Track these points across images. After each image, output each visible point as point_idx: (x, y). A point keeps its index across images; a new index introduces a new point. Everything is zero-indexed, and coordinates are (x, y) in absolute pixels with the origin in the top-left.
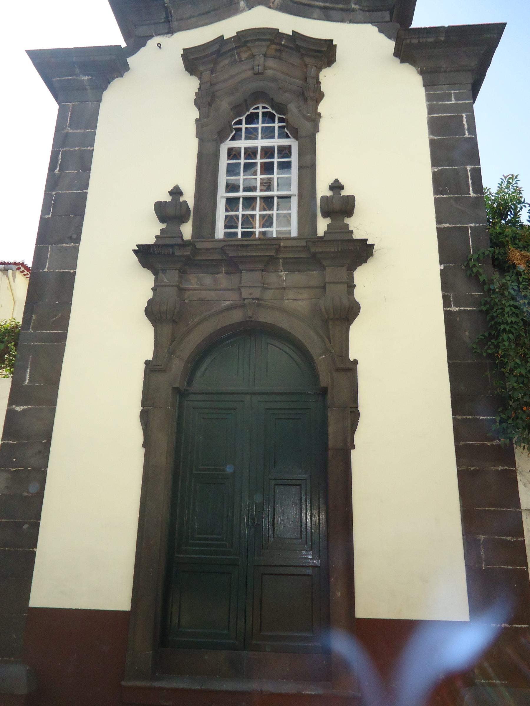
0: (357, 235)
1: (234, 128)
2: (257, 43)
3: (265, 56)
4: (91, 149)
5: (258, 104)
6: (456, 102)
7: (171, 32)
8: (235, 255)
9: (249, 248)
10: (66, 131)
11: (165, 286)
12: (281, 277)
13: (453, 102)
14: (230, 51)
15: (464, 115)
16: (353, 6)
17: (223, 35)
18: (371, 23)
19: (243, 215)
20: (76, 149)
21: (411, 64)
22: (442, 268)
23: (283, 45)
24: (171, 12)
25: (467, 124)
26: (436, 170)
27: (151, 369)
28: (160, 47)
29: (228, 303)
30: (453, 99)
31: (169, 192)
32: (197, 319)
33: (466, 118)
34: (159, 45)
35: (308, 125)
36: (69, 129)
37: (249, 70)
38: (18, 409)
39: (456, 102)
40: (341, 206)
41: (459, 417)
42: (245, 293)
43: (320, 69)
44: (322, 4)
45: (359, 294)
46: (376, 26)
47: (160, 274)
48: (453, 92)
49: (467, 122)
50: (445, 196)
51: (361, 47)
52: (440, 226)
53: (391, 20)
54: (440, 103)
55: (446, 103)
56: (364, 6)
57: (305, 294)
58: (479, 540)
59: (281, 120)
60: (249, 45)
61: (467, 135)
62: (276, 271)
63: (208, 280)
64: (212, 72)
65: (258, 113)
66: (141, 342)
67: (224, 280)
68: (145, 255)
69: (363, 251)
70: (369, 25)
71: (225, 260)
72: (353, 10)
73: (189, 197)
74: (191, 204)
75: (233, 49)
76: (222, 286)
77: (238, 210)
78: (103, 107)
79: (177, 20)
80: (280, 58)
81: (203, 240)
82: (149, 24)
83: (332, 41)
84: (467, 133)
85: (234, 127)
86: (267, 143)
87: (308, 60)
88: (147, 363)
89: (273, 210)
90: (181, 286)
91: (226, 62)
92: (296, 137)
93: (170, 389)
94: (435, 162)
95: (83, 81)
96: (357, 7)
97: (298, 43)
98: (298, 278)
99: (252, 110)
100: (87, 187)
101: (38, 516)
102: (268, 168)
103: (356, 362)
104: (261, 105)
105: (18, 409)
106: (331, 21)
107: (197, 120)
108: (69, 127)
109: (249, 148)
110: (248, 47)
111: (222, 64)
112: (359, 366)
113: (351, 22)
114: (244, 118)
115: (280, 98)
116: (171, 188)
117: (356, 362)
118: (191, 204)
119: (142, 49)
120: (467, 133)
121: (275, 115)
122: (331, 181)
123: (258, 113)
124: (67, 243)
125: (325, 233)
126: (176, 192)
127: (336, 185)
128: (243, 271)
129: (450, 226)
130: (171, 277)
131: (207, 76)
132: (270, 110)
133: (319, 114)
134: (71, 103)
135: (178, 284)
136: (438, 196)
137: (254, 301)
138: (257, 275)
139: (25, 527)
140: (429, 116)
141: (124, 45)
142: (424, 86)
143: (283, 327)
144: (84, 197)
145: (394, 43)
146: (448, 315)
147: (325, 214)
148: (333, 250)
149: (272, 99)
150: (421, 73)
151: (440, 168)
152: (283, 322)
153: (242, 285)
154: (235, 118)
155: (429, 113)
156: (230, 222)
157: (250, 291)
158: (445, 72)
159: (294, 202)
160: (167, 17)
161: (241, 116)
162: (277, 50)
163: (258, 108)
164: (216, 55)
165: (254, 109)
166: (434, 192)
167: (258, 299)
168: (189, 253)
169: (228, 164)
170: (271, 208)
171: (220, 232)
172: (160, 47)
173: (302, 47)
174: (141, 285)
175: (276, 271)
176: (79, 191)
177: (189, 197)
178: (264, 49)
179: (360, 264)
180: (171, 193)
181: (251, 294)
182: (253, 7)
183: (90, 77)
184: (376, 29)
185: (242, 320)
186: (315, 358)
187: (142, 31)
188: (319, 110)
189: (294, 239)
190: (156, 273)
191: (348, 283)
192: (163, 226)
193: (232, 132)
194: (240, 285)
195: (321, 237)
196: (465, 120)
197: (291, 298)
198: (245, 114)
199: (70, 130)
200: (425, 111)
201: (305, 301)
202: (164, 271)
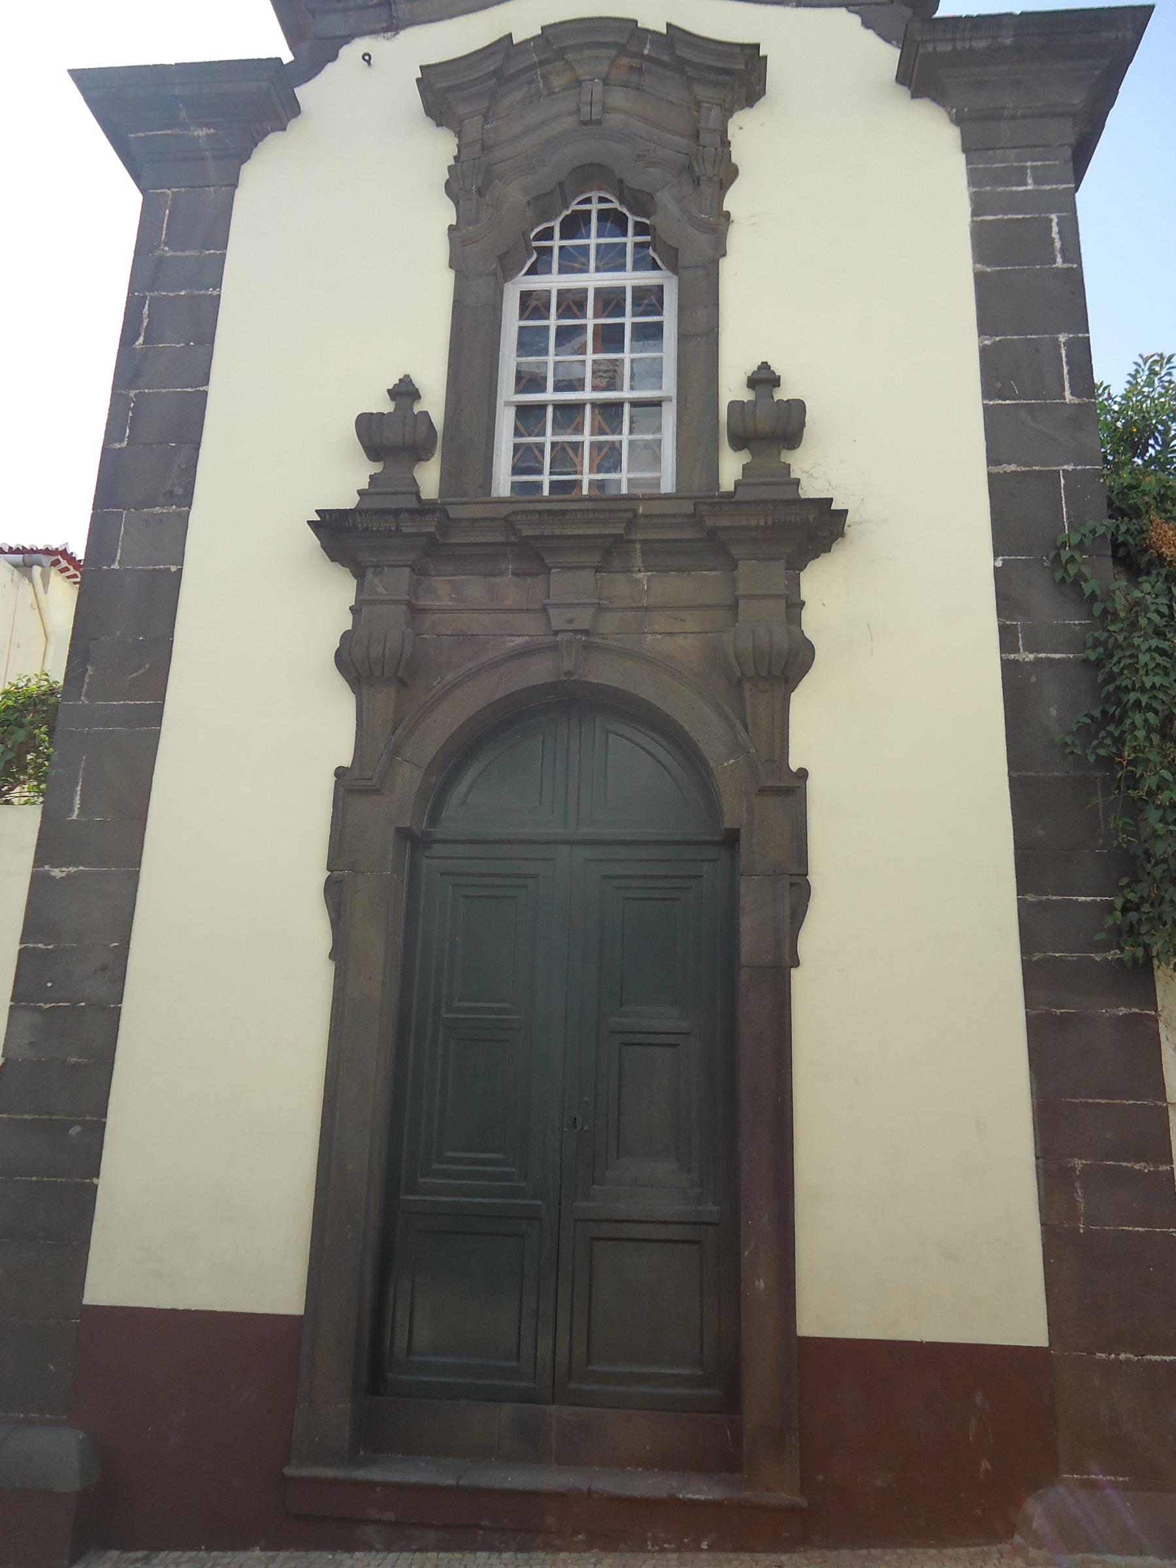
0: (810, 490)
1: (536, 248)
2: (587, 53)
4: (215, 293)
8: (537, 533)
11: (381, 602)
12: (638, 582)
13: (1030, 187)
15: (1054, 217)
18: (846, 6)
19: (553, 444)
20: (182, 293)
22: (999, 564)
25: (1061, 239)
26: (987, 342)
28: (369, 62)
30: (1030, 181)
34: (367, 58)
35: (702, 239)
38: (57, 873)
40: (774, 424)
41: (1030, 898)
42: (558, 619)
43: (728, 113)
46: (856, 13)
48: (1029, 164)
49: (1059, 233)
50: (1007, 402)
52: (995, 470)
54: (1000, 189)
55: (1014, 189)
58: (1073, 1169)
59: (641, 229)
60: (569, 56)
62: (628, 571)
63: (475, 588)
64: (486, 118)
65: (589, 212)
66: (327, 727)
67: (511, 589)
68: (336, 532)
69: (822, 526)
71: (512, 544)
73: (433, 402)
75: (532, 67)
77: (542, 433)
81: (464, 499)
83: (757, 47)
84: (1059, 259)
85: (535, 244)
86: (609, 279)
87: (702, 92)
88: (340, 772)
89: (621, 433)
90: (414, 601)
91: (518, 95)
92: (674, 268)
99: (574, 207)
101: (102, 1111)
102: (610, 338)
103: (803, 774)
104: (595, 195)
105: (57, 873)
108: (166, 244)
109: (568, 291)
110: (567, 62)
112: (811, 783)
114: (556, 224)
116: (392, 381)
117: (803, 774)
120: (1059, 259)
123: (589, 212)
124: (163, 507)
125: (737, 484)
126: (404, 392)
127: (764, 375)
132: (616, 205)
133: (728, 214)
135: (407, 597)
138: (586, 578)
139: (75, 1130)
141: (287, 57)
142: (964, 151)
144: (201, 400)
145: (899, 52)
147: (739, 442)
148: (754, 523)
150: (957, 120)
151: (998, 339)
152: (644, 685)
154: (537, 225)
155: (974, 213)
156: (526, 460)
158: (1013, 118)
159: (669, 415)
161: (551, 220)
162: (631, 69)
163: (588, 201)
164: (494, 80)
167: (586, 632)
168: (432, 529)
169: (521, 328)
171: (503, 482)
172: (369, 62)
174: (326, 602)
177: (433, 402)
178: (603, 68)
181: (571, 621)
183: (212, 131)
184: (856, 19)
188: (727, 205)
189: (667, 497)
190: (359, 574)
191: (787, 597)
192: (376, 468)
193: (530, 255)
194: (547, 601)
195: (729, 495)
196: (1055, 229)
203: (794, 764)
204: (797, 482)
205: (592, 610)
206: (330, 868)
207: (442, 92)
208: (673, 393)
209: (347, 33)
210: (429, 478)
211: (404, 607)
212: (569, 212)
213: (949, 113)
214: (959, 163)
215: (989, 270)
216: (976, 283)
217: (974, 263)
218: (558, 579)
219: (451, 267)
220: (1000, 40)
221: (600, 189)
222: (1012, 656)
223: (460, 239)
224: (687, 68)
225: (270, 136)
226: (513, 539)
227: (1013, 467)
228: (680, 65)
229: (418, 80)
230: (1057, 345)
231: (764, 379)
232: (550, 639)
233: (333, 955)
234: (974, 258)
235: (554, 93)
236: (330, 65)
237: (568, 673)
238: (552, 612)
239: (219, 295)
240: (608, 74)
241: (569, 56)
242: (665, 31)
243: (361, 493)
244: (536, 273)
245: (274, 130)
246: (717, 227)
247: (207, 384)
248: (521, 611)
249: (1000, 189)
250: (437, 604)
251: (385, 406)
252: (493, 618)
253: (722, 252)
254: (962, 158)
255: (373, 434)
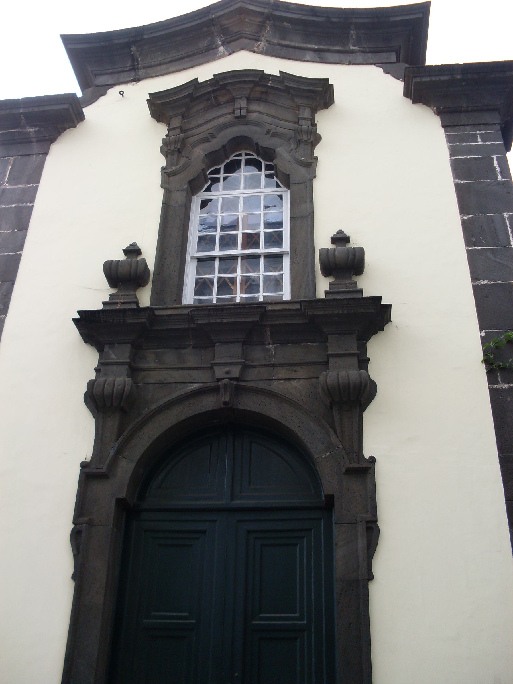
1: (210, 179)
2: (238, 86)
3: (249, 100)
4: (31, 205)
5: (241, 150)
6: (483, 143)
7: (137, 80)
8: (207, 321)
9: (225, 312)
10: (3, 187)
11: (112, 364)
12: (269, 350)
13: (480, 143)
14: (204, 94)
16: (352, 48)
17: (197, 79)
18: (375, 64)
19: (219, 279)
20: (13, 206)
21: (424, 104)
22: (483, 334)
23: (269, 86)
24: (137, 60)
25: (499, 167)
26: (465, 218)
27: (90, 475)
28: (122, 95)
29: (196, 386)
30: (479, 140)
31: (124, 250)
32: (154, 407)
33: (497, 160)
34: (122, 93)
35: (302, 170)
36: (7, 185)
37: (229, 113)
39: (483, 143)
40: (346, 262)
42: (219, 372)
43: (314, 111)
44: (316, 47)
45: (375, 372)
46: (380, 67)
47: (106, 349)
48: (478, 132)
49: (498, 164)
50: (479, 248)
51: (364, 93)
52: (476, 283)
53: (398, 61)
54: (464, 144)
55: (471, 144)
56: (365, 48)
57: (302, 372)
59: (268, 168)
60: (229, 88)
61: (500, 178)
62: (262, 344)
63: (170, 357)
64: (184, 117)
65: (240, 160)
67: (191, 358)
68: (89, 324)
70: (373, 68)
72: (352, 52)
73: (149, 256)
74: (151, 265)
75: (209, 93)
76: (189, 364)
77: (212, 272)
78: (49, 160)
79: (145, 68)
80: (266, 101)
81: (165, 306)
82: (111, 73)
83: (327, 80)
84: (500, 176)
85: (210, 176)
87: (298, 101)
89: (259, 271)
91: (202, 106)
92: (287, 185)
93: (114, 501)
94: (463, 209)
95: (28, 133)
96: (356, 48)
97: (286, 84)
98: (295, 353)
99: (232, 158)
100: (21, 248)
103: (372, 460)
104: (243, 152)
106: (327, 63)
107: (163, 169)
108: (7, 183)
110: (227, 90)
111: (195, 109)
113: (350, 64)
114: (222, 167)
115: (266, 142)
116: (126, 245)
117: (372, 460)
118: (151, 265)
119: (102, 98)
120: (500, 176)
121: (261, 163)
122: (333, 232)
123: (240, 160)
125: (326, 293)
126: (133, 251)
127: (339, 236)
128: (217, 344)
129: (489, 283)
130: (121, 353)
131: (176, 122)
132: (255, 156)
133: (316, 158)
134: (12, 157)
135: (128, 360)
136: (470, 248)
137: (232, 382)
138: (237, 349)
140: (452, 158)
141: (79, 94)
142: (443, 126)
143: (272, 416)
144: (17, 259)
145: (402, 83)
146: (494, 394)
147: (327, 271)
148: (336, 312)
149: (257, 144)
150: (439, 113)
151: (471, 216)
152: (272, 410)
153: (217, 361)
154: (211, 167)
155: (451, 155)
156: (203, 287)
157: (227, 369)
158: (467, 111)
159: (287, 262)
160: (133, 65)
161: (219, 164)
162: (262, 93)
163: (240, 155)
164: (188, 99)
165: (234, 156)
166: (465, 243)
167: (237, 379)
168: (144, 320)
170: (256, 268)
171: (189, 298)
172: (122, 95)
173: (292, 88)
174: (82, 363)
175: (262, 344)
176: (12, 254)
177: (149, 256)
178: (247, 92)
179: (375, 333)
180: (127, 252)
181: (227, 373)
182: (234, 52)
183: (38, 129)
184: (381, 70)
185: (215, 408)
186: (316, 456)
187: (102, 80)
188: (315, 154)
189: (287, 302)
190: (100, 350)
193: (206, 182)
194: (212, 362)
196: (496, 162)
197: (287, 386)
198: (223, 162)
199: (7, 186)
200: (447, 154)
201: (301, 382)
202: (112, 344)
203: (367, 454)
204: (361, 291)
205: (240, 367)
206: (74, 523)
207: (161, 106)
208: (289, 250)
209: (112, 83)
210: (145, 298)
211: (126, 367)
212: (229, 161)
213: (433, 110)
214: (441, 132)
215: (462, 182)
216: (456, 188)
217: (454, 179)
218: (220, 349)
219: (162, 187)
220: (454, 76)
221: (246, 149)
222: (495, 386)
223: (167, 174)
224: (291, 90)
225: (67, 130)
226: (192, 326)
227: (486, 282)
228: (287, 89)
229: (148, 100)
230: (504, 219)
231: (341, 239)
232: (215, 384)
233: (74, 577)
234: (453, 177)
235: (221, 105)
236: (102, 97)
237: (225, 403)
238: (216, 368)
239: (33, 206)
240: (249, 95)
241: (229, 88)
242: (279, 75)
243: (104, 303)
244: (210, 191)
245: (70, 127)
246: (310, 165)
247: (22, 250)
248: (197, 368)
249: (464, 144)
250: (147, 365)
251: (121, 257)
252: (181, 378)
253: (314, 176)
254: (442, 130)
255: (114, 274)
